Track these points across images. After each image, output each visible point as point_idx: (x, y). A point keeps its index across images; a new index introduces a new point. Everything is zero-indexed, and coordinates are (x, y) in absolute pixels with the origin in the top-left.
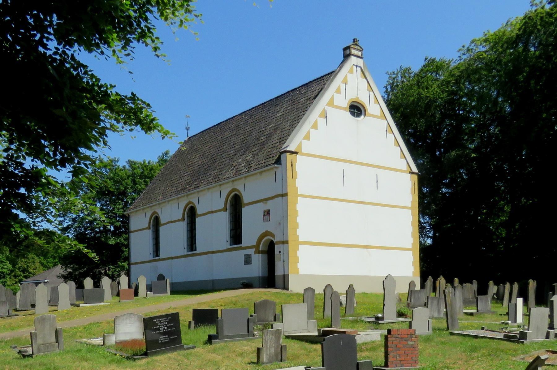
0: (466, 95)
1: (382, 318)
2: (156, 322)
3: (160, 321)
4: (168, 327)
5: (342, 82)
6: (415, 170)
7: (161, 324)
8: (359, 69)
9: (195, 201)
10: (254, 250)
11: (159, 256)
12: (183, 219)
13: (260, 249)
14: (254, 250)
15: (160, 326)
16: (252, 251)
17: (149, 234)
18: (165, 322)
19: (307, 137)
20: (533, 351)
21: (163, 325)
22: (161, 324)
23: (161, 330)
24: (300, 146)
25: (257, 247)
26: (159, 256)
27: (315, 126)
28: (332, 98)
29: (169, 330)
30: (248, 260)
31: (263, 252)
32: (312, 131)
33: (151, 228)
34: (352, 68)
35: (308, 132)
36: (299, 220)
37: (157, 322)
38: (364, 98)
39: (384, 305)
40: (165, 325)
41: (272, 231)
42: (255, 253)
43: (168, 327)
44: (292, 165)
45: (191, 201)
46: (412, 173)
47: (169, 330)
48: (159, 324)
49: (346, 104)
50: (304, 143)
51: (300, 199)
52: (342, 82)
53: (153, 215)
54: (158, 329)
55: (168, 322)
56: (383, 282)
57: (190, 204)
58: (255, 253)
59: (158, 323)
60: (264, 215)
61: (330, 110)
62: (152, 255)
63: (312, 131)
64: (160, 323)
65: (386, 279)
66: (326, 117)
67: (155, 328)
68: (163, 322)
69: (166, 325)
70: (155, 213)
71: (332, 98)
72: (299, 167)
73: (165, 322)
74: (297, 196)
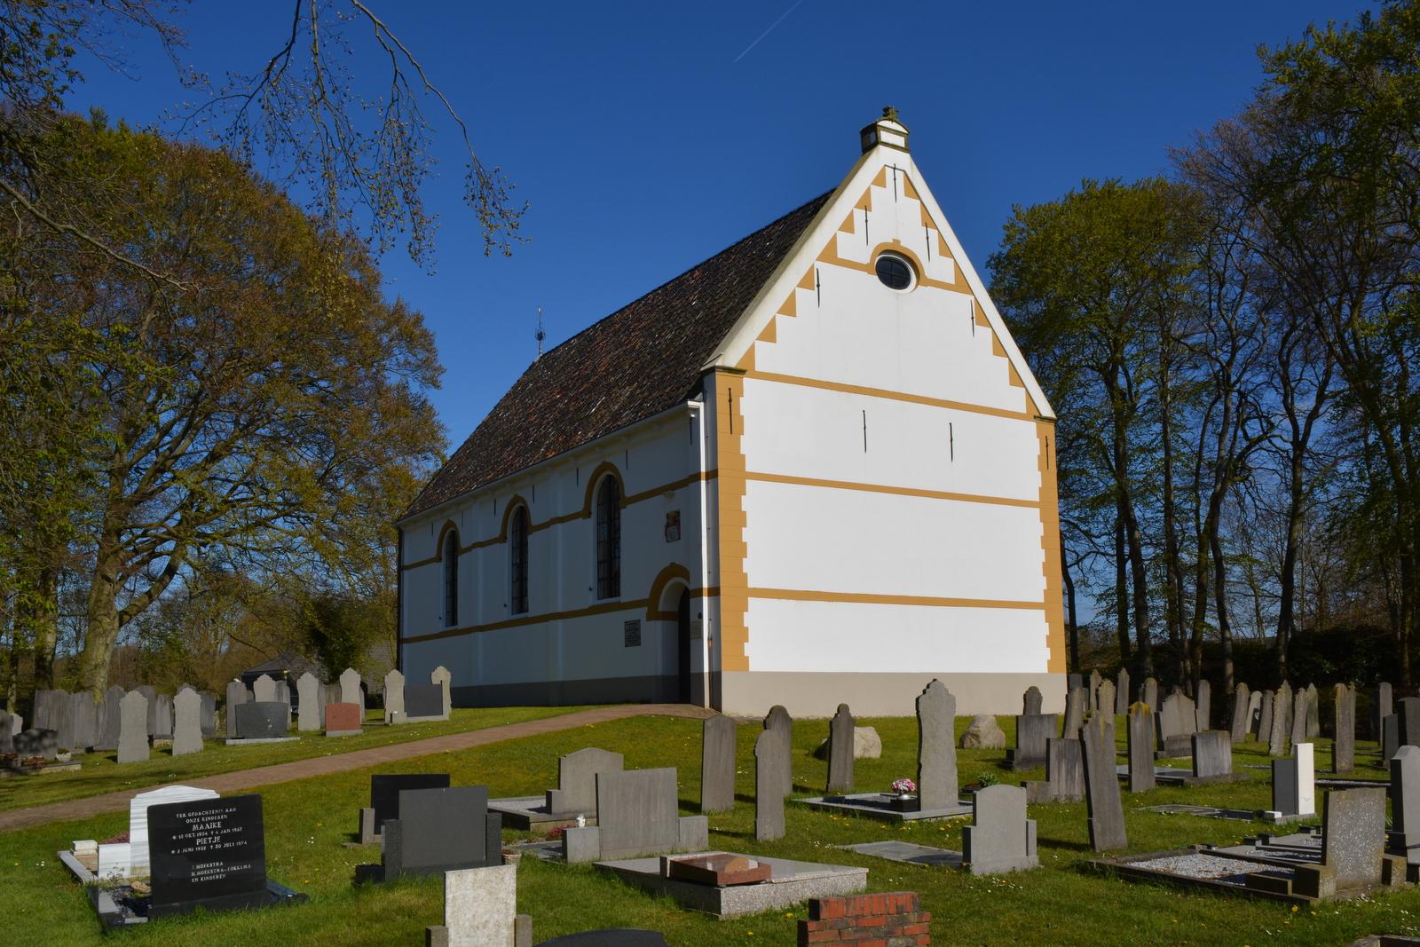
0: (1398, 164)
1: (915, 805)
2: (184, 819)
3: (201, 816)
4: (224, 839)
5: (857, 206)
6: (1047, 410)
7: (202, 827)
8: (900, 175)
9: (618, 461)
10: (645, 609)
11: (527, 611)
12: (586, 513)
13: (660, 609)
14: (645, 609)
15: (197, 832)
16: (639, 614)
17: (587, 532)
18: (214, 821)
19: (769, 334)
20: (879, 891)
21: (209, 831)
22: (202, 827)
23: (200, 845)
24: (751, 353)
25: (651, 603)
26: (527, 611)
27: (789, 308)
28: (833, 243)
29: (227, 845)
30: (633, 636)
31: (665, 616)
32: (805, 297)
33: (594, 516)
34: (882, 173)
35: (772, 324)
36: (747, 535)
37: (188, 821)
38: (913, 241)
39: (920, 766)
40: (214, 830)
41: (657, 573)
42: (649, 618)
43: (224, 839)
44: (730, 401)
45: (608, 460)
46: (1039, 418)
47: (227, 845)
48: (195, 827)
49: (865, 255)
50: (762, 348)
51: (750, 484)
52: (857, 206)
53: (603, 471)
54: (192, 842)
55: (225, 824)
56: (917, 700)
57: (605, 470)
58: (649, 618)
59: (192, 824)
60: (668, 526)
61: (827, 271)
62: (595, 592)
63: (782, 321)
64: (201, 822)
65: (924, 692)
66: (818, 286)
67: (181, 837)
68: (209, 822)
69: (219, 830)
70: (606, 466)
71: (833, 243)
72: (746, 406)
73: (214, 821)
74: (743, 476)
